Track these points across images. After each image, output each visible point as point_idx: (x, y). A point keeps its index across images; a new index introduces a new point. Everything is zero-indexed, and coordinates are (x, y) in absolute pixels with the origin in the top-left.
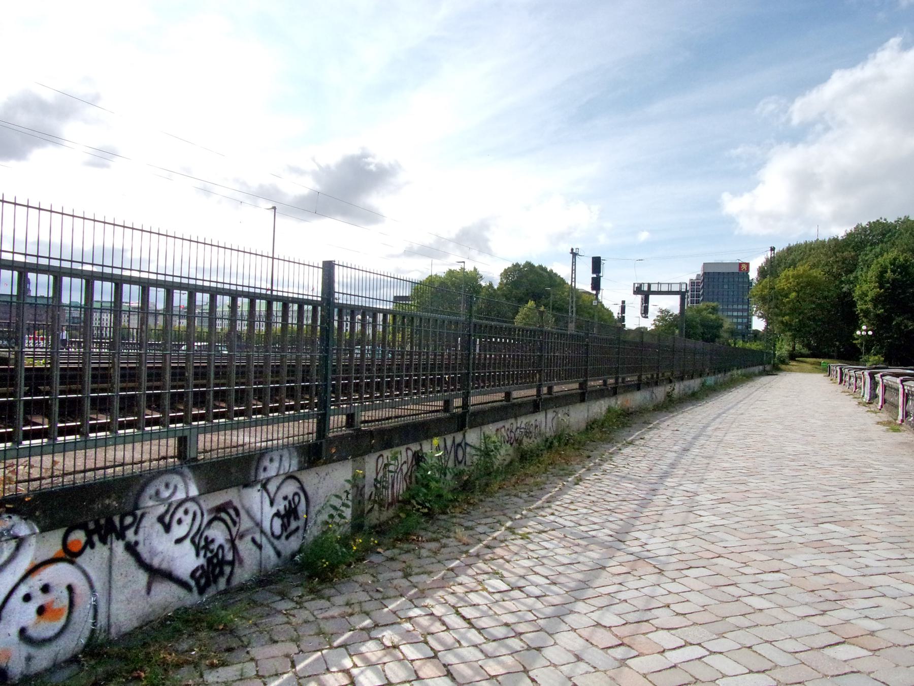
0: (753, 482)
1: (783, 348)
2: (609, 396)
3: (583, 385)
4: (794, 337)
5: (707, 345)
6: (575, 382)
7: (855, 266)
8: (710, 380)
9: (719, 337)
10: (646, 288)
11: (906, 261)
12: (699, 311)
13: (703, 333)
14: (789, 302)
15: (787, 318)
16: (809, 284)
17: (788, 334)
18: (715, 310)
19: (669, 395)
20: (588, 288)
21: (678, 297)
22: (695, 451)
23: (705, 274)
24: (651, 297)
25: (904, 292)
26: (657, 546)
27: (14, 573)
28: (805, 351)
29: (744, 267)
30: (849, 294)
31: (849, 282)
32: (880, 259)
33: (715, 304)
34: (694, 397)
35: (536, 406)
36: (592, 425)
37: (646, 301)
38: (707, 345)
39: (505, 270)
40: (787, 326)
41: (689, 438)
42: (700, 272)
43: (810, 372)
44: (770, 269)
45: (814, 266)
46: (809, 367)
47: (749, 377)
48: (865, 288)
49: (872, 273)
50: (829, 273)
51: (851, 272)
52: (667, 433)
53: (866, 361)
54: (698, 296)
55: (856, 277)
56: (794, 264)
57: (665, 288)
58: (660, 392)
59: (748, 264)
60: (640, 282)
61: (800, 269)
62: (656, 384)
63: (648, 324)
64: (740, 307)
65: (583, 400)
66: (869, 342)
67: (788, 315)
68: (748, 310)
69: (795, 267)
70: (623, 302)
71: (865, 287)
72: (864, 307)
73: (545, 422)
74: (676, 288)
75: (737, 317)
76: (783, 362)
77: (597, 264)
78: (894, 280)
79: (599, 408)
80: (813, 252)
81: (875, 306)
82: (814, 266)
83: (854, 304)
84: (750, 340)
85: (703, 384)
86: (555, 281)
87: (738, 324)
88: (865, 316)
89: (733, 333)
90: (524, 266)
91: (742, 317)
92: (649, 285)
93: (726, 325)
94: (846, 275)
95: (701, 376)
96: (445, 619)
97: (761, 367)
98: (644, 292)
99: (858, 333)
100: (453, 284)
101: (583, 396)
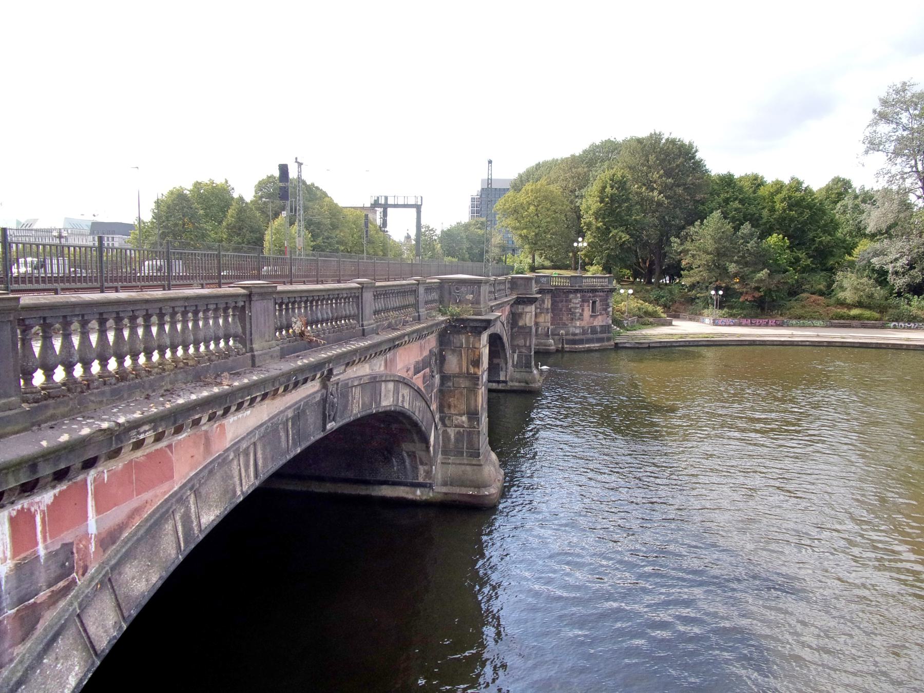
11: (623, 177)
15: (525, 231)
16: (546, 198)
24: (389, 210)
25: (620, 206)
27: (407, 493)
39: (260, 183)
48: (590, 203)
57: (401, 202)
81: (597, 219)
86: (315, 195)
92: (386, 198)
94: (579, 189)
100: (200, 196)
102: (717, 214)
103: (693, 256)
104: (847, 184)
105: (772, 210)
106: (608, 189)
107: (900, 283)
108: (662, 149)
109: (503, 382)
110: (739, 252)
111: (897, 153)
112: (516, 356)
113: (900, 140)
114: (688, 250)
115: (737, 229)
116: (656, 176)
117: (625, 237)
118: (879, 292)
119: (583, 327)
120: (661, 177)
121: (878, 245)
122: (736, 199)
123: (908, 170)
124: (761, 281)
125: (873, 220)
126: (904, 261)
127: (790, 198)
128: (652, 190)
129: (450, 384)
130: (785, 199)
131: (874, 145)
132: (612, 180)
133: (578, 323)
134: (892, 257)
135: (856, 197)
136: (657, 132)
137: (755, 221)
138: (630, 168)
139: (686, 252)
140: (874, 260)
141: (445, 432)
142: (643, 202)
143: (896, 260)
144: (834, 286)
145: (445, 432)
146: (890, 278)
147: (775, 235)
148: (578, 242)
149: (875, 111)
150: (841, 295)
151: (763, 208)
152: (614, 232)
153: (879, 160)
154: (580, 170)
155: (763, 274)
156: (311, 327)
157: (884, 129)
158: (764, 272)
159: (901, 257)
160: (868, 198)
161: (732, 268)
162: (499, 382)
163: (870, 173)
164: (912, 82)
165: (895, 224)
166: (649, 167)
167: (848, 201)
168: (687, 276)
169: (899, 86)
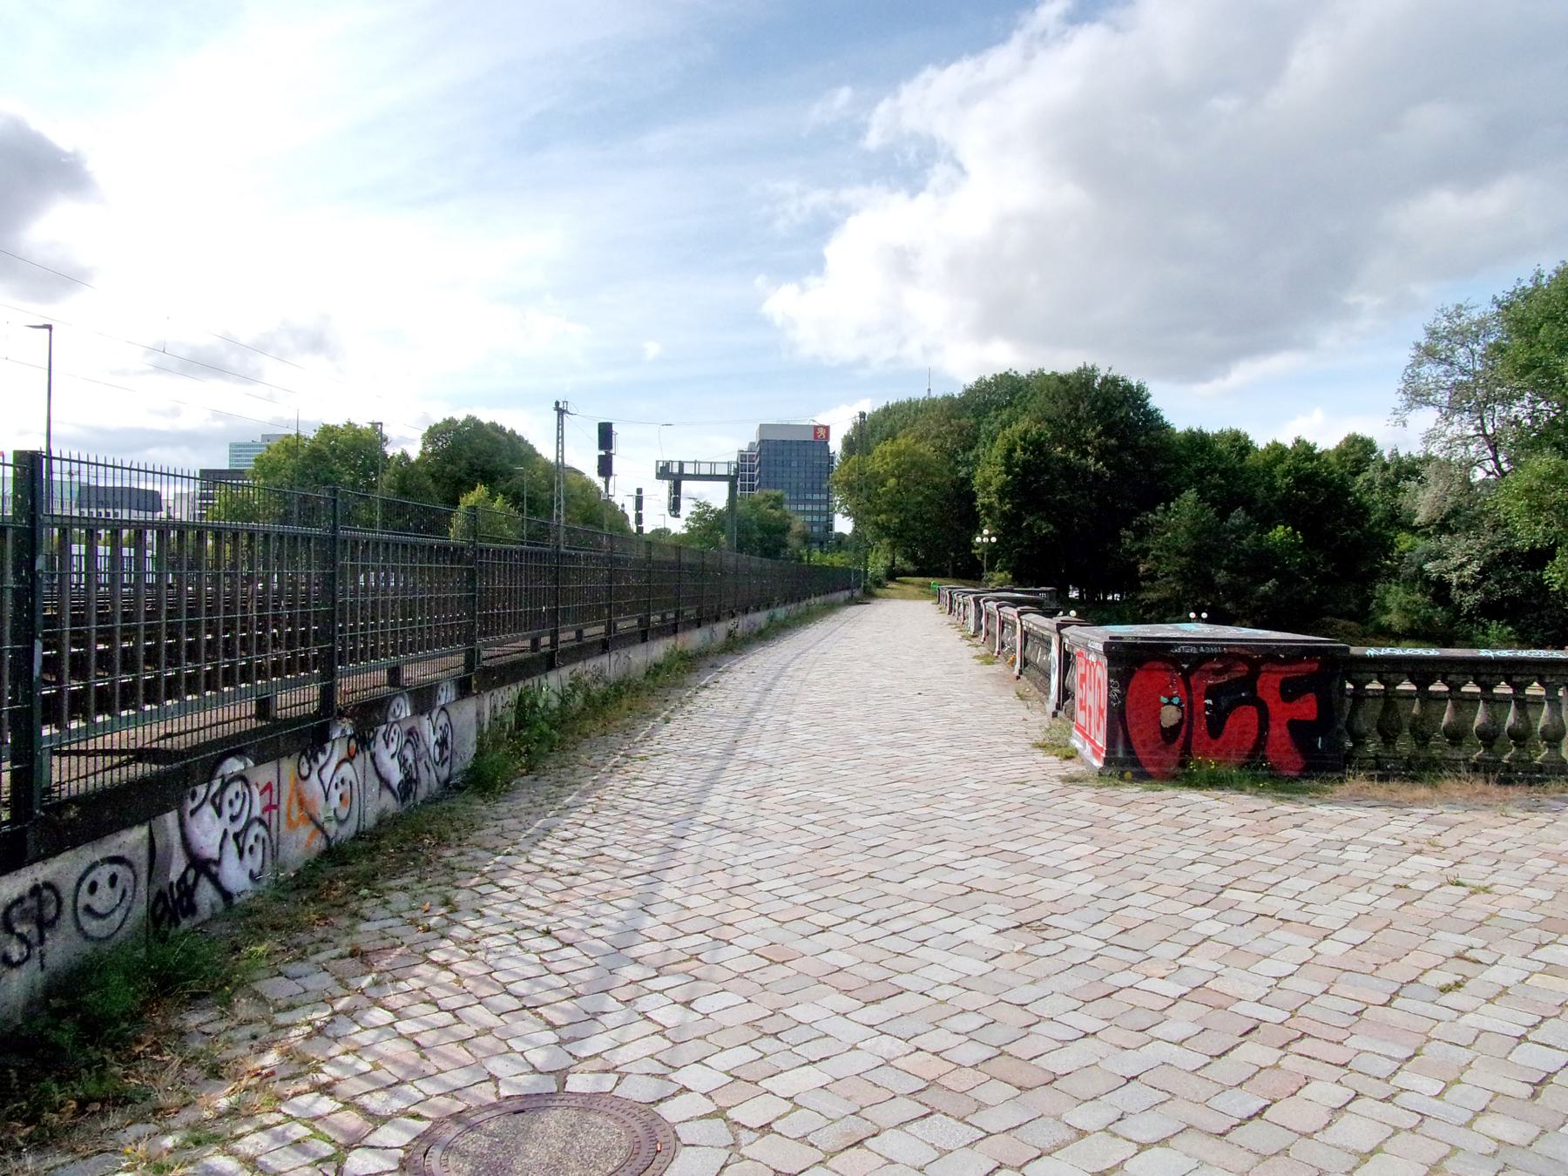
0: (839, 711)
1: (878, 563)
2: (668, 635)
3: (611, 627)
4: (893, 546)
5: (767, 559)
6: (524, 638)
7: (976, 438)
8: (780, 613)
9: (785, 546)
10: (676, 470)
12: (755, 505)
13: (761, 540)
14: (885, 493)
15: (883, 517)
17: (886, 541)
18: (778, 502)
19: (730, 634)
20: (590, 470)
21: (725, 485)
22: (777, 690)
23: (762, 442)
24: (684, 483)
25: (1036, 481)
26: (760, 753)
28: (909, 566)
29: (822, 432)
30: (966, 481)
31: (967, 463)
32: (1007, 431)
33: (778, 492)
34: (763, 636)
35: (605, 646)
36: (655, 670)
37: (676, 489)
38: (767, 559)
40: (884, 529)
41: (769, 680)
42: (755, 439)
43: (916, 597)
44: (859, 441)
45: (921, 438)
46: (916, 591)
47: (831, 608)
48: (988, 474)
49: (997, 452)
50: (941, 448)
51: (971, 448)
52: (743, 676)
53: (991, 580)
54: (752, 478)
55: (977, 456)
56: (892, 435)
57: (705, 470)
58: (721, 629)
59: (827, 428)
60: (667, 459)
61: (902, 442)
62: (718, 619)
63: (677, 526)
64: (816, 497)
65: (644, 640)
66: (993, 553)
67: (885, 512)
68: (828, 501)
69: (894, 439)
70: (639, 491)
71: (988, 473)
72: (986, 501)
73: (610, 665)
74: (722, 470)
75: (812, 513)
76: (879, 584)
77: (606, 435)
78: (1024, 462)
79: (659, 649)
80: (920, 416)
81: (1001, 500)
82: (921, 438)
83: (973, 496)
84: (831, 550)
85: (771, 618)
87: (813, 523)
88: (987, 515)
89: (807, 539)
90: (465, 424)
91: (819, 513)
92: (681, 464)
93: (798, 524)
94: (964, 451)
95: (768, 606)
96: (434, 969)
97: (847, 593)
98: (673, 476)
99: (978, 539)
101: (644, 635)
102: (1190, 495)
103: (1157, 558)
104: (1367, 446)
105: (1271, 488)
106: (1018, 454)
107: (1471, 599)
108: (1098, 394)
110: (1229, 553)
111: (1454, 408)
113: (1458, 387)
114: (1149, 549)
115: (1224, 514)
116: (1091, 434)
117: (1047, 528)
118: (1440, 615)
120: (1099, 436)
121: (1432, 545)
122: (1215, 470)
123: (1472, 432)
124: (1265, 596)
125: (1423, 503)
126: (1474, 567)
127: (1297, 470)
128: (1085, 454)
130: (1289, 472)
131: (1417, 396)
132: (1023, 439)
134: (1454, 561)
135: (1386, 467)
136: (1089, 366)
137: (1248, 502)
138: (1049, 421)
139: (1145, 552)
140: (1428, 566)
142: (1069, 470)
143: (1462, 566)
144: (1373, 606)
146: (1455, 594)
147: (1280, 527)
149: (1418, 346)
150: (1384, 620)
151: (1258, 485)
152: (1030, 519)
153: (1426, 418)
154: (963, 421)
155: (1268, 586)
157: (1431, 371)
158: (1270, 583)
159: (1470, 561)
160: (1409, 470)
161: (1221, 577)
163: (1404, 432)
164: (1470, 303)
165: (1455, 512)
166: (1078, 420)
167: (1371, 472)
168: (1150, 590)
169: (1451, 309)
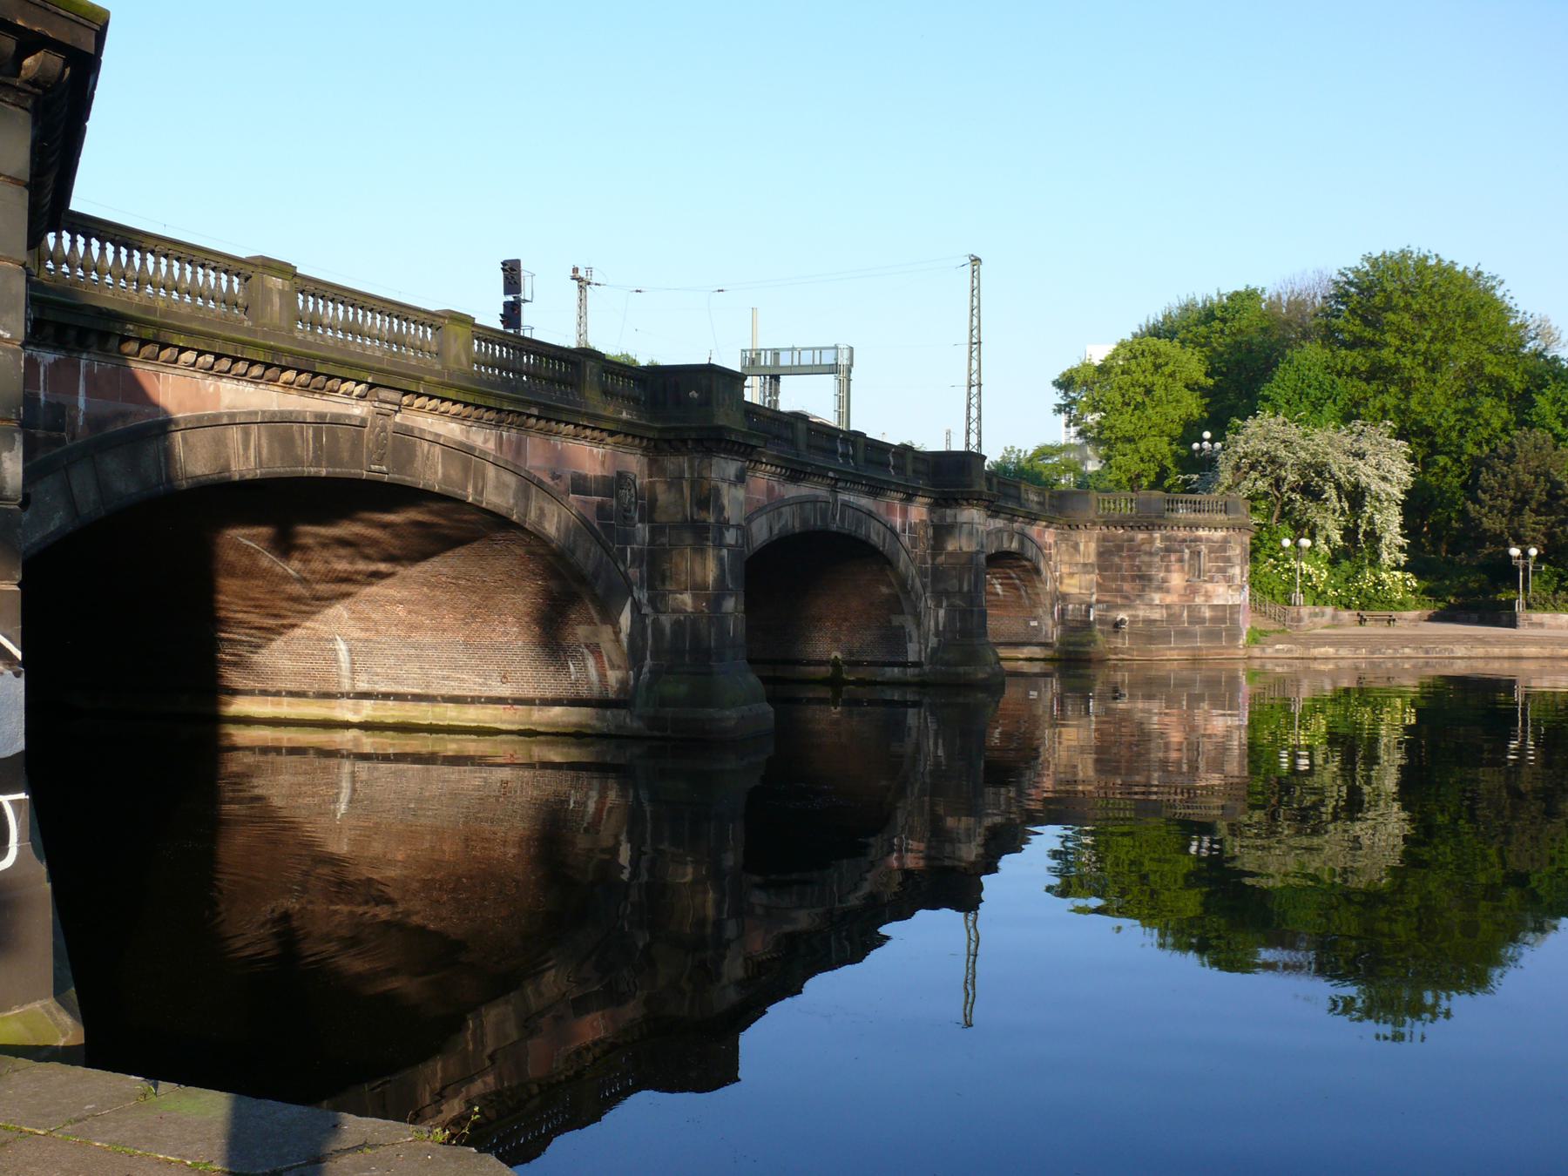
109: (915, 665)
112: (942, 612)
119: (1168, 607)
129: (665, 540)
133: (1157, 598)
141: (656, 622)
145: (656, 622)
148: (1201, 440)
156: (355, 338)
162: (904, 665)
